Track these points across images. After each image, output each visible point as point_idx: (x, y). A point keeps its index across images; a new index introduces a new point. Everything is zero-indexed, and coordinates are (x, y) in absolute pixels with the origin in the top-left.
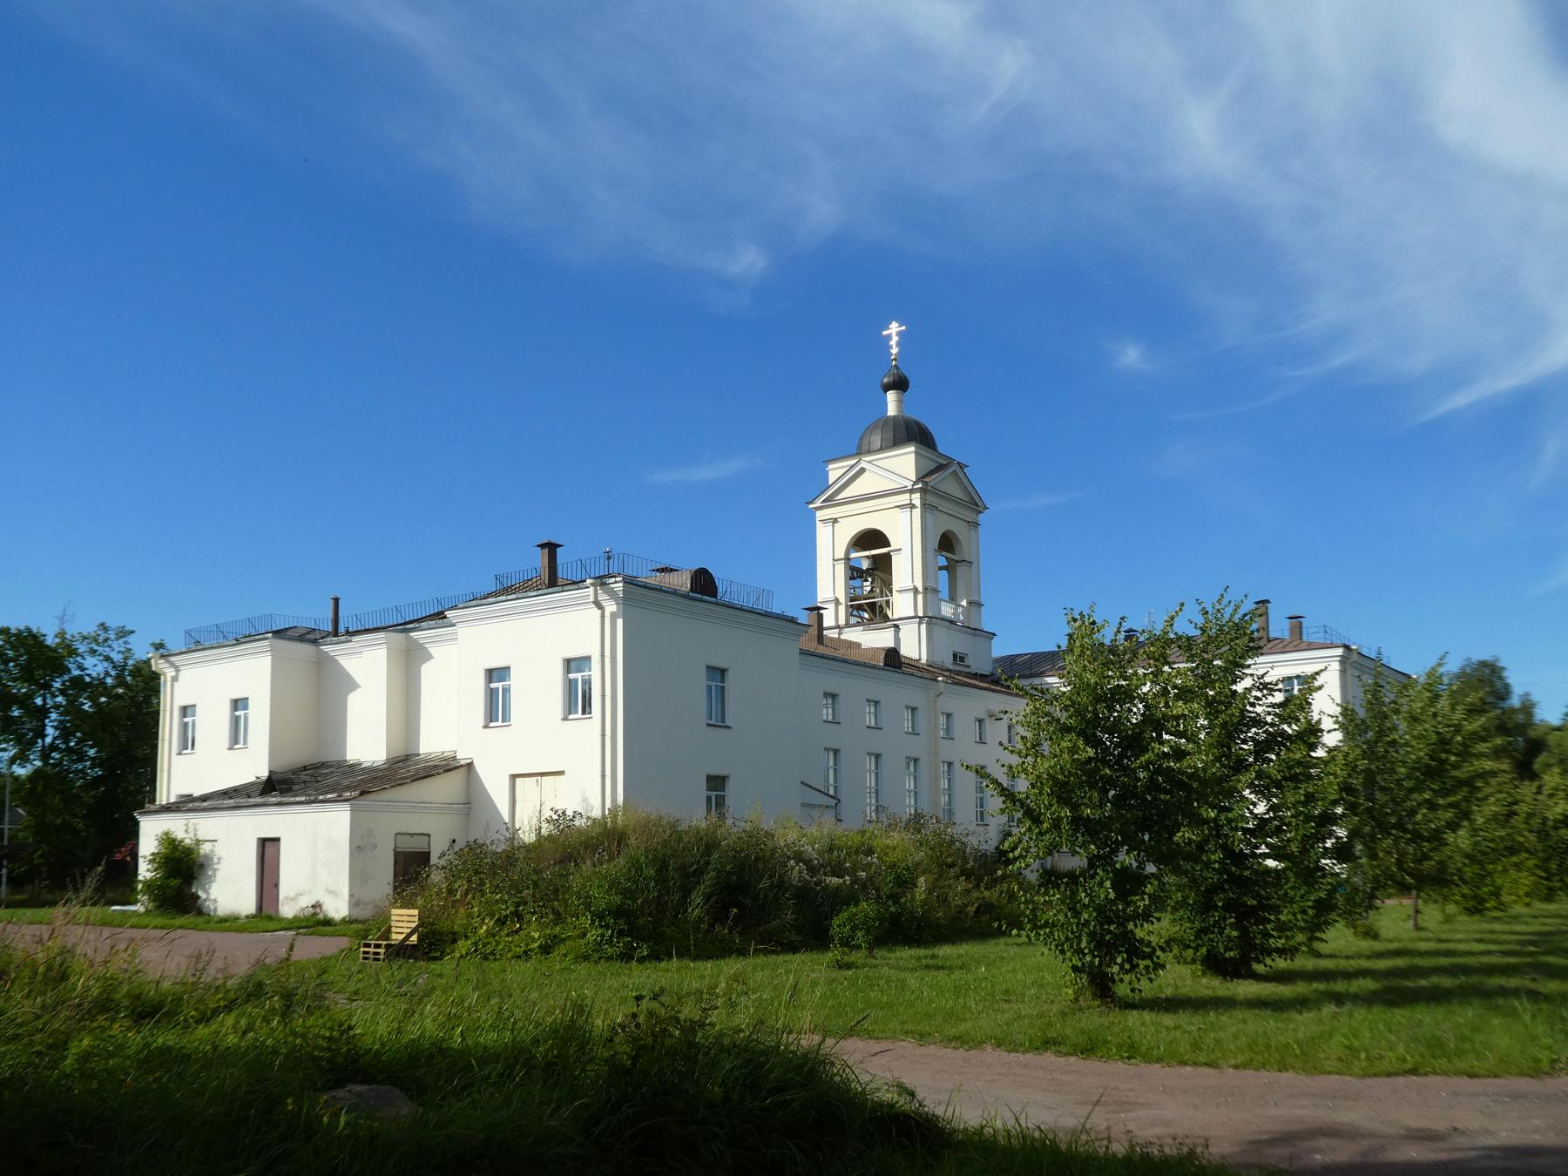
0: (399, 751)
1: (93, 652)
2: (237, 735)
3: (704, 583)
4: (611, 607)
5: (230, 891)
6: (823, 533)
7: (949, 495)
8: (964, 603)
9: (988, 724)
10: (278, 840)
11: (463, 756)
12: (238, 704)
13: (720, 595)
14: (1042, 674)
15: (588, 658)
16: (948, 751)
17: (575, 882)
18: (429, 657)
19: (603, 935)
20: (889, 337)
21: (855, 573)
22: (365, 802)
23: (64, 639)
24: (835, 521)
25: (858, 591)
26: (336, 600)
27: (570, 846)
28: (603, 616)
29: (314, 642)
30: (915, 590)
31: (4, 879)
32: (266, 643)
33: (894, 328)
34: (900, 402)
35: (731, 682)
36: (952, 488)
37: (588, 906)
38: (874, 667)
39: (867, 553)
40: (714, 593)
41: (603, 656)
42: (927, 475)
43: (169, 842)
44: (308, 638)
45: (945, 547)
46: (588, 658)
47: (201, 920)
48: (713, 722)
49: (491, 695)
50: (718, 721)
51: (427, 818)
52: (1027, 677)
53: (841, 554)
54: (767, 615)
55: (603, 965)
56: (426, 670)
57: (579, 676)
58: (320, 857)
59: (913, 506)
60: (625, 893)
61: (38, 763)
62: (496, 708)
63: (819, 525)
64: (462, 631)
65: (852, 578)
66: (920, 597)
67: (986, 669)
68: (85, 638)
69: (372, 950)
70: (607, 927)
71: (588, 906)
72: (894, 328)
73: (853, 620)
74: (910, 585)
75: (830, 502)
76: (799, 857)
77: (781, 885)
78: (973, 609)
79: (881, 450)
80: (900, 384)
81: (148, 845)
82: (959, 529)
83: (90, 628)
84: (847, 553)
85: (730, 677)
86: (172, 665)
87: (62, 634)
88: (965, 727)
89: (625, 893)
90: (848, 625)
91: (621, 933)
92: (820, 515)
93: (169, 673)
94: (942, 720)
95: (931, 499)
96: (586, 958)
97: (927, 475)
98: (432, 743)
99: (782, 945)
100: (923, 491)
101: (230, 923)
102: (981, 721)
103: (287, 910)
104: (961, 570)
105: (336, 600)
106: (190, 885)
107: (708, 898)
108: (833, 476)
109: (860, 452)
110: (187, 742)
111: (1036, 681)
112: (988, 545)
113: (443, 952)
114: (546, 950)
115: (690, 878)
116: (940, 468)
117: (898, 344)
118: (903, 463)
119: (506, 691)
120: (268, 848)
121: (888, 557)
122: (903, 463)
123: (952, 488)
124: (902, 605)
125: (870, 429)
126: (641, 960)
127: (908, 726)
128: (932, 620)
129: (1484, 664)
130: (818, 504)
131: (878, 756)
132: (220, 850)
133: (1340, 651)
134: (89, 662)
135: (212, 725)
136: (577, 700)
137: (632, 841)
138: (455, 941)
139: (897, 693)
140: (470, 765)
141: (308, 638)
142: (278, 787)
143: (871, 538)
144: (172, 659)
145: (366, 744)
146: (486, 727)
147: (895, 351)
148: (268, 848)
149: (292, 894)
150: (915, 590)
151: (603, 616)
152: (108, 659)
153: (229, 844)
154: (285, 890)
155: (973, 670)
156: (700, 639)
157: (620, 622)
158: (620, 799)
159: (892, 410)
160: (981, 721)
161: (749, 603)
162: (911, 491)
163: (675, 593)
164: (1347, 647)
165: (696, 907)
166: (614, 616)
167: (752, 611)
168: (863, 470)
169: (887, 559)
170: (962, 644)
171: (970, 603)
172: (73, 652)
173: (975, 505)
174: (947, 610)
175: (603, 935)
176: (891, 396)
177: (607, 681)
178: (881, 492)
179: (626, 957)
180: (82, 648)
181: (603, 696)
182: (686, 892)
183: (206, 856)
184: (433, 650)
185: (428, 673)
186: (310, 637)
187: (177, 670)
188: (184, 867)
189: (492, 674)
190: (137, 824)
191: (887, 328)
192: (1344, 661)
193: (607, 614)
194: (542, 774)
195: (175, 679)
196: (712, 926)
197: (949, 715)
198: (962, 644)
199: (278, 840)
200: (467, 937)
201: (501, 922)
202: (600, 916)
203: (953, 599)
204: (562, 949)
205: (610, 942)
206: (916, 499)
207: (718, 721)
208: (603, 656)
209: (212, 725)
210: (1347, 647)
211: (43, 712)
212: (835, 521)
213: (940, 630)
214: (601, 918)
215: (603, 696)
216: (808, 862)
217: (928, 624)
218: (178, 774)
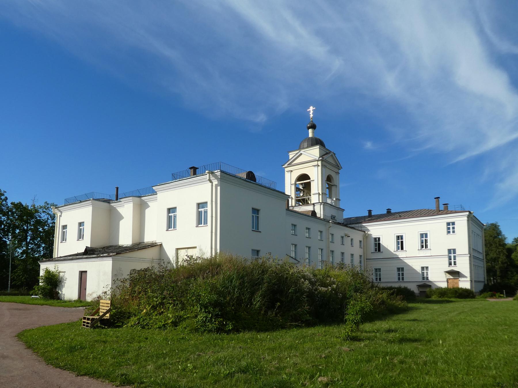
0: (137, 241)
1: (44, 212)
2: (81, 236)
3: (251, 176)
4: (215, 182)
5: (69, 291)
6: (287, 175)
7: (329, 162)
8: (334, 199)
9: (345, 238)
10: (86, 272)
11: (158, 241)
12: (81, 224)
13: (257, 181)
14: (361, 223)
15: (206, 203)
16: (332, 247)
17: (193, 287)
18: (148, 206)
19: (207, 317)
20: (310, 111)
21: (297, 189)
22: (119, 257)
23: (34, 207)
24: (291, 171)
25: (298, 196)
26: (117, 188)
27: (196, 270)
28: (212, 186)
29: (109, 203)
30: (319, 194)
31: (9, 286)
32: (90, 202)
33: (311, 109)
34: (313, 133)
35: (261, 215)
36: (331, 160)
37: (198, 300)
38: (308, 216)
39: (302, 182)
40: (255, 180)
41: (212, 201)
42: (324, 155)
43: (48, 272)
44: (107, 201)
45: (329, 181)
46: (206, 203)
47: (55, 301)
48: (254, 229)
49: (169, 218)
50: (256, 228)
51: (142, 261)
52: (356, 224)
53: (293, 182)
54: (274, 190)
55: (206, 336)
56: (147, 211)
57: (203, 210)
58: (100, 279)
59: (318, 166)
60: (220, 294)
61: (25, 248)
62: (171, 223)
63: (286, 173)
64: (160, 195)
65: (297, 191)
66: (321, 196)
67: (341, 221)
68: (41, 207)
69: (86, 321)
70: (209, 312)
71: (198, 300)
72: (311, 109)
73: (297, 205)
74: (317, 192)
75: (290, 165)
76: (304, 277)
77: (300, 291)
78: (337, 201)
79: (307, 147)
80: (313, 127)
81: (42, 273)
82: (333, 174)
83: (43, 204)
84: (295, 182)
85: (261, 213)
86: (60, 211)
87: (34, 206)
88: (337, 239)
89: (220, 294)
90: (295, 206)
91: (217, 316)
92: (286, 169)
93: (59, 214)
94: (330, 236)
95: (324, 163)
96: (197, 330)
97: (324, 155)
98: (148, 239)
99: (302, 322)
100: (322, 160)
101: (70, 304)
102: (342, 237)
103: (89, 299)
104: (333, 188)
105: (117, 188)
106: (56, 288)
107: (263, 296)
108: (291, 157)
109: (300, 148)
110: (64, 239)
111: (360, 225)
112: (342, 182)
113: (123, 323)
114: (175, 324)
115: (255, 285)
116: (327, 154)
117: (313, 113)
118: (315, 152)
119: (175, 216)
120: (83, 274)
121: (309, 183)
122: (315, 152)
123: (331, 160)
124: (314, 199)
125: (304, 141)
126: (228, 332)
127: (319, 238)
128: (324, 204)
129: (492, 224)
130: (286, 166)
131: (309, 248)
132: (66, 276)
133: (467, 213)
134: (43, 215)
135: (72, 232)
136: (201, 219)
137: (225, 268)
138: (129, 318)
139: (315, 227)
140: (161, 245)
141: (107, 201)
142: (89, 253)
143: (304, 177)
144: (60, 209)
145: (125, 239)
146: (167, 230)
147: (311, 116)
148: (83, 274)
149: (91, 293)
150: (319, 194)
151: (212, 186)
152: (48, 214)
153: (69, 273)
154: (88, 291)
155: (338, 221)
156: (252, 198)
157: (219, 188)
158: (218, 251)
159: (310, 135)
160: (342, 237)
161: (267, 185)
162: (318, 161)
163: (240, 178)
164: (470, 212)
165: (257, 301)
166: (216, 186)
167: (269, 188)
168: (301, 154)
169: (309, 184)
170: (334, 212)
171: (336, 199)
172: (37, 211)
173: (338, 167)
174: (329, 201)
175: (207, 317)
176: (310, 131)
177: (213, 212)
178: (307, 162)
179: (220, 330)
180: (40, 210)
181: (212, 217)
182: (253, 294)
183: (62, 278)
184: (150, 204)
185: (148, 213)
186: (108, 201)
187: (61, 213)
188: (54, 281)
189: (170, 210)
190: (39, 266)
191: (309, 108)
192: (468, 217)
193: (214, 185)
194: (188, 248)
195: (60, 216)
196: (266, 312)
197: (332, 235)
198: (334, 212)
199: (86, 272)
200: (135, 315)
201: (154, 308)
202: (205, 306)
203: (330, 197)
204: (184, 324)
205: (210, 321)
206: (320, 163)
207: (256, 228)
208: (212, 201)
209: (72, 232)
210: (470, 212)
211: (26, 231)
212: (291, 171)
213: (327, 208)
214: (206, 308)
215: (212, 217)
216: (310, 280)
217: (324, 205)
218: (61, 249)
